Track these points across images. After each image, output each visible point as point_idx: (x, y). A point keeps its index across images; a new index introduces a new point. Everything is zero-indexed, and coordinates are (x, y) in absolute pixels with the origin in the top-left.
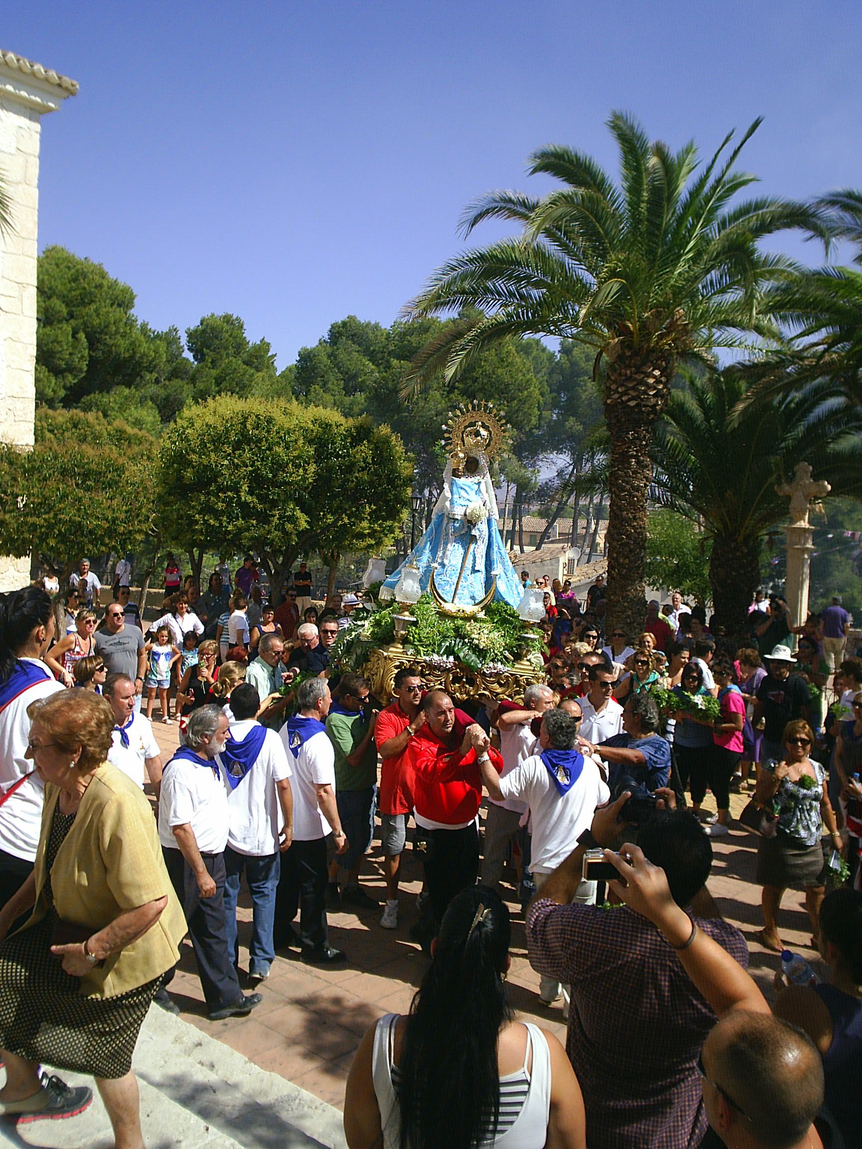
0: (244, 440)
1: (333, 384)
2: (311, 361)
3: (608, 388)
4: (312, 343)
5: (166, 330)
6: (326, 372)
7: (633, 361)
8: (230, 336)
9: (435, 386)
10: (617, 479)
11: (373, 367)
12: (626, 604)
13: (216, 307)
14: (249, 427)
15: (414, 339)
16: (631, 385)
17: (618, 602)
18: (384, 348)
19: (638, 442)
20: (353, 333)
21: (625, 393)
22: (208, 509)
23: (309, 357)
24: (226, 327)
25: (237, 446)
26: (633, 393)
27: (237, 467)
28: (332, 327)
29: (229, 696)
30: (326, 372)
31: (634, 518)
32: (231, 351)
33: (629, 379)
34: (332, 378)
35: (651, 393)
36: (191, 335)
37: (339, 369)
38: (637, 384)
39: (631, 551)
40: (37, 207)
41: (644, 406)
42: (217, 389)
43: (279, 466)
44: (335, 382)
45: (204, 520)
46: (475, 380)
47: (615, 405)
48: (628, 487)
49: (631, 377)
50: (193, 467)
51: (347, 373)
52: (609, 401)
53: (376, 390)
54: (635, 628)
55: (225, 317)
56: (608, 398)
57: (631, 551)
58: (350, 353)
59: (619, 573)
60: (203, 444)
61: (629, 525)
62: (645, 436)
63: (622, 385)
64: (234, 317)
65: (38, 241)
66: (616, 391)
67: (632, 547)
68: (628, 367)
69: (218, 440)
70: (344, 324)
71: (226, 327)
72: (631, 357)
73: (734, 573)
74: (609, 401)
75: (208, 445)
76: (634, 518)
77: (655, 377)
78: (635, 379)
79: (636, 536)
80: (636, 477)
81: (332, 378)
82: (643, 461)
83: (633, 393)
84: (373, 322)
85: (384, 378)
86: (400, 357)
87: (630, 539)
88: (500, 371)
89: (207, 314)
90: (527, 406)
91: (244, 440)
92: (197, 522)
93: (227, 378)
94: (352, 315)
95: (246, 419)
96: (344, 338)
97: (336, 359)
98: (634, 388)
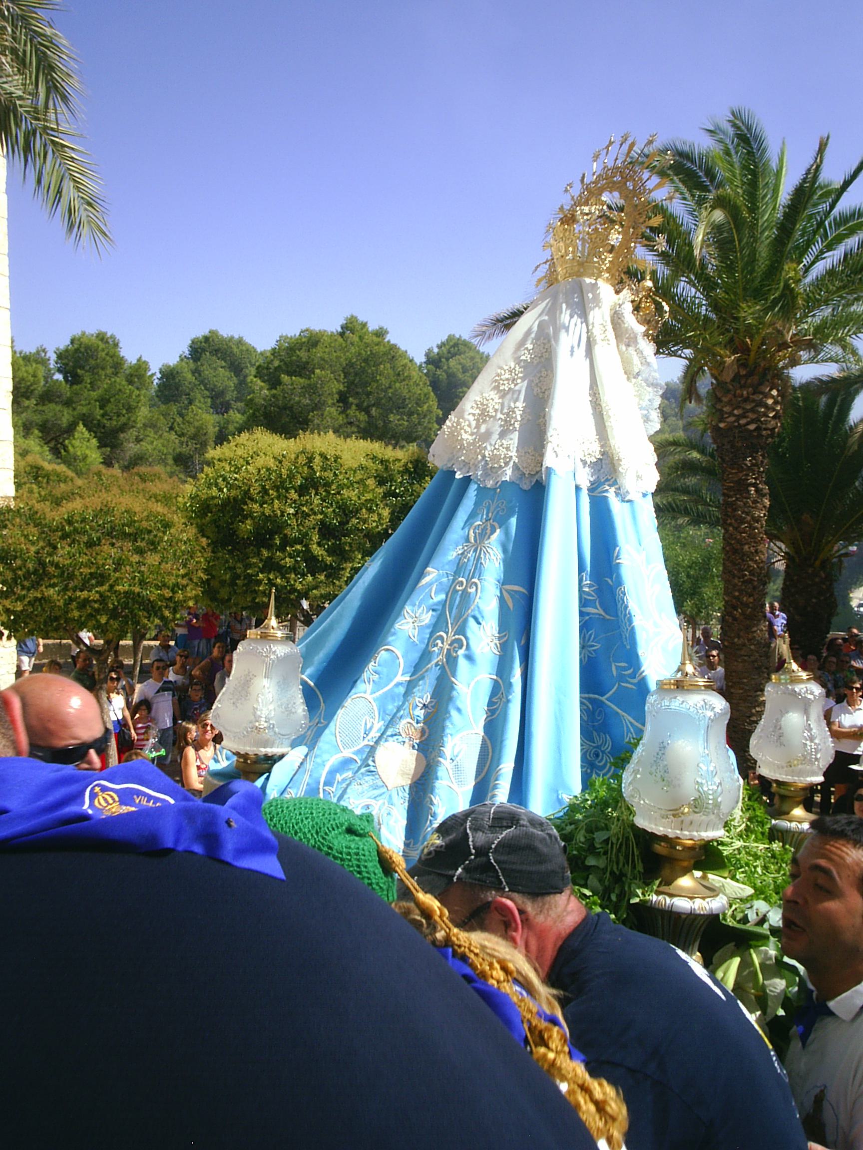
0: (310, 484)
1: (200, 402)
2: (174, 378)
3: (721, 411)
4: (173, 360)
5: (34, 351)
6: (192, 390)
7: (749, 381)
8: (107, 354)
9: (330, 402)
10: (735, 510)
11: (262, 384)
12: (752, 647)
13: (87, 324)
14: (317, 468)
15: (303, 354)
16: (748, 407)
17: (744, 645)
18: (269, 363)
19: (756, 468)
20: (216, 348)
21: (743, 416)
22: (271, 566)
23: (172, 374)
24: (102, 345)
25: (302, 491)
26: (751, 416)
27: (306, 516)
28: (193, 342)
29: (563, 844)
30: (192, 390)
31: (756, 551)
32: (109, 371)
33: (746, 400)
34: (199, 396)
35: (771, 415)
36: (60, 356)
37: (205, 386)
38: (756, 406)
39: (754, 588)
40: (6, 216)
41: (765, 429)
42: (102, 412)
43: (346, 511)
44: (202, 400)
45: (269, 579)
46: (369, 394)
47: (730, 428)
48: (749, 518)
49: (748, 398)
50: (253, 518)
51: (213, 390)
52: (722, 425)
53: (265, 407)
54: (763, 672)
55: (98, 335)
56: (721, 422)
57: (754, 588)
58: (215, 369)
59: (743, 614)
60: (265, 491)
61: (752, 560)
62: (762, 462)
63: (738, 407)
64: (109, 335)
65: (9, 255)
66: (731, 414)
67: (756, 583)
68: (743, 387)
69: (281, 486)
70: (206, 339)
71: (102, 345)
72: (747, 376)
73: (814, 600)
74: (722, 425)
75: (271, 492)
76: (756, 551)
77: (773, 397)
78: (754, 401)
79: (758, 571)
80: (756, 507)
81: (199, 396)
82: (762, 490)
83: (751, 416)
84: (236, 337)
85: (274, 396)
86: (290, 374)
87: (753, 575)
88: (398, 385)
89: (77, 332)
90: (426, 420)
91: (310, 484)
92: (259, 582)
93: (112, 400)
94: (214, 329)
95: (310, 460)
96: (208, 354)
97: (200, 375)
98: (753, 410)
